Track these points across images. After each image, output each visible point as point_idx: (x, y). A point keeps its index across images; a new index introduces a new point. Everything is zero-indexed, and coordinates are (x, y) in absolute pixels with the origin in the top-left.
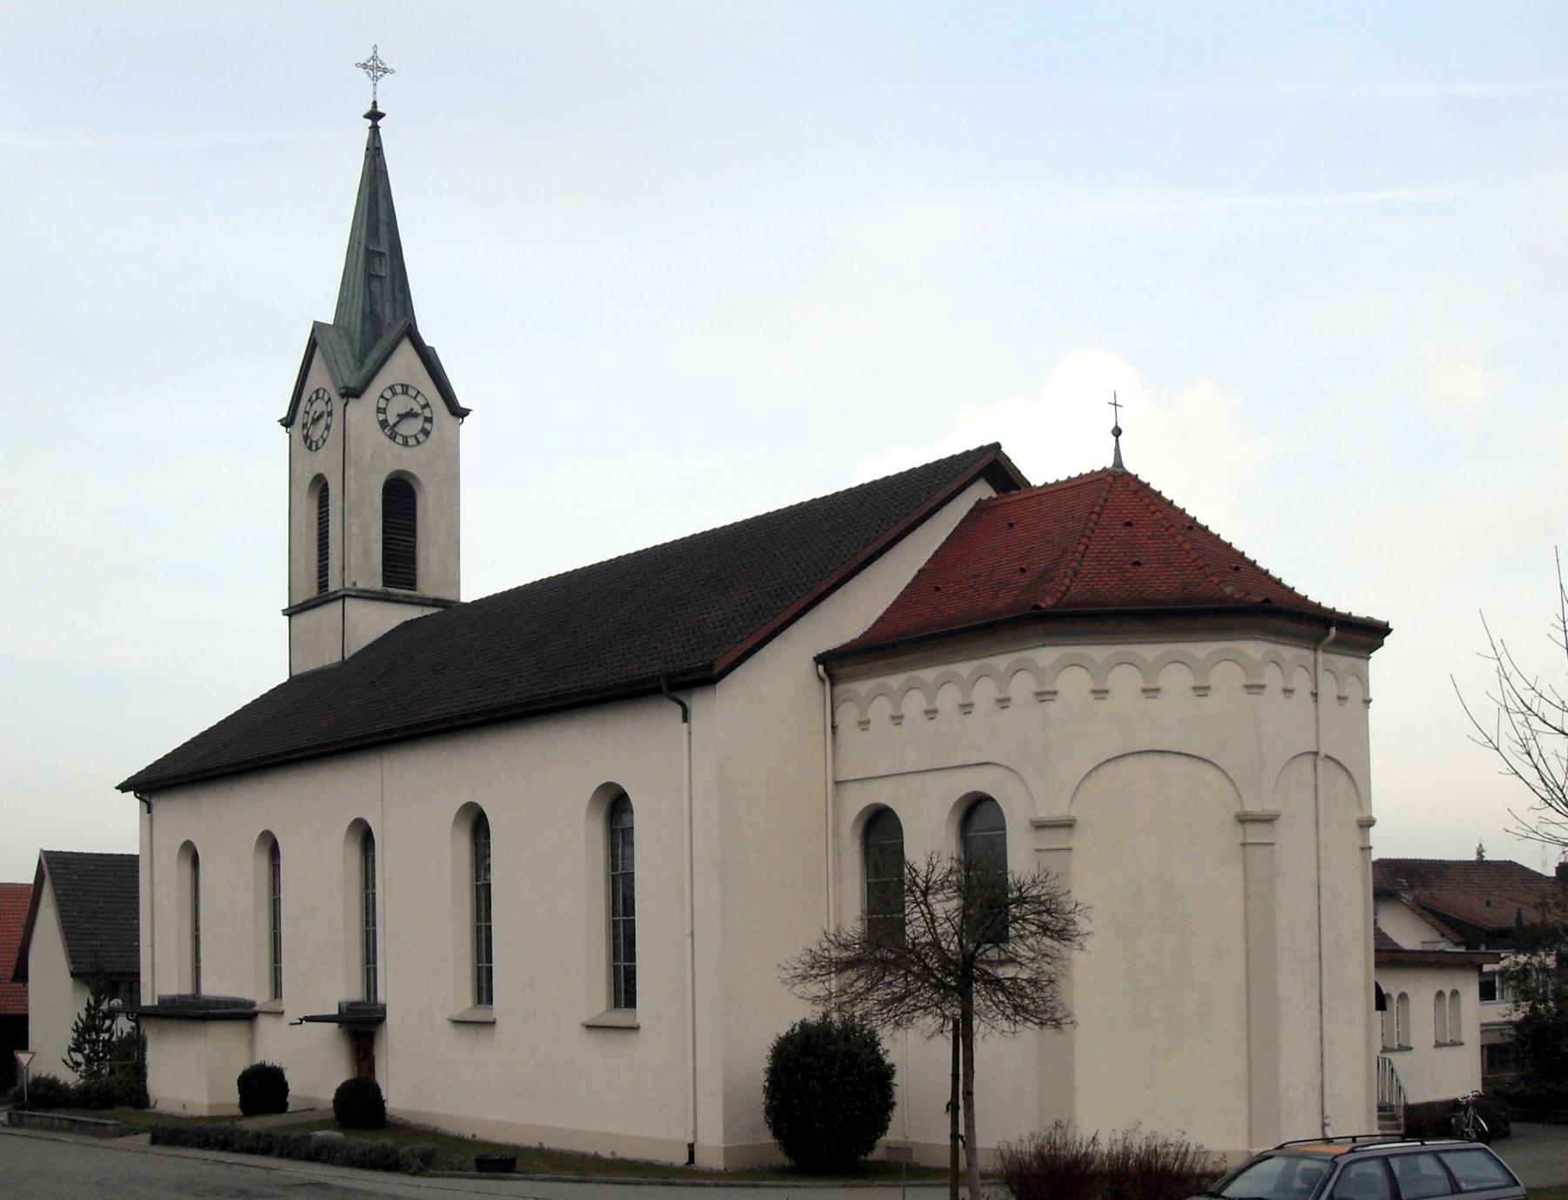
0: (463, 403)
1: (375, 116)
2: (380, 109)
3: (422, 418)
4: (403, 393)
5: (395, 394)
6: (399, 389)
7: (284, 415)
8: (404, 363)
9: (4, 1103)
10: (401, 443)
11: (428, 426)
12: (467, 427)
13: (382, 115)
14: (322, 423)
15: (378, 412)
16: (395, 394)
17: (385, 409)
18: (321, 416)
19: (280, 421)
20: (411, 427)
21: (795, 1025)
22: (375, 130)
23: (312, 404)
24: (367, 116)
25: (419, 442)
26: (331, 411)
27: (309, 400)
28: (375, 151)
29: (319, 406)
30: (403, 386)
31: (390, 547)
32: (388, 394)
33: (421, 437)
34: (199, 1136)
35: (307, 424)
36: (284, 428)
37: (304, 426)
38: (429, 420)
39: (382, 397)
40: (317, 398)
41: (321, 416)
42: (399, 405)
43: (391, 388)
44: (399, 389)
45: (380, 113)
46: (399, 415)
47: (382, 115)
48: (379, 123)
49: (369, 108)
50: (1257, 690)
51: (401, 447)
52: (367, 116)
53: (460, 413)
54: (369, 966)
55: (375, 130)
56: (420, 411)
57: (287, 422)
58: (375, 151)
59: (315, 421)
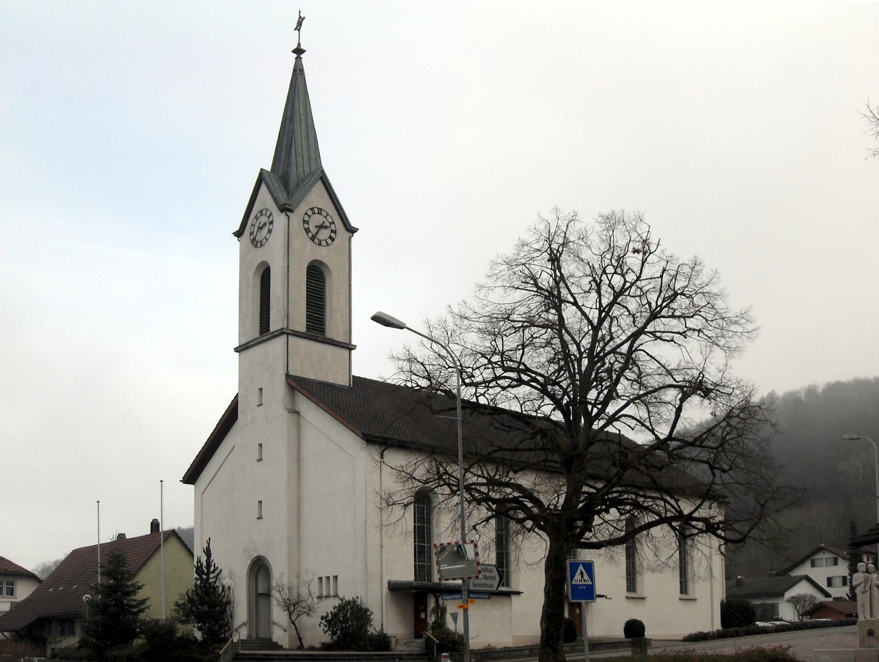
0: (354, 224)
1: (299, 51)
2: (303, 47)
3: (329, 230)
4: (318, 213)
5: (314, 213)
6: (316, 211)
7: (238, 228)
8: (316, 197)
9: (877, 621)
10: (317, 243)
11: (333, 235)
12: (356, 238)
13: (303, 51)
14: (266, 230)
15: (304, 223)
16: (314, 213)
17: (308, 222)
18: (265, 224)
19: (234, 233)
20: (324, 234)
21: (189, 590)
22: (298, 59)
23: (257, 220)
24: (294, 51)
25: (328, 245)
26: (273, 221)
27: (255, 217)
28: (298, 72)
29: (263, 219)
30: (318, 209)
31: (310, 304)
32: (310, 213)
33: (329, 241)
34: (380, 637)
35: (253, 232)
36: (237, 238)
37: (251, 233)
38: (334, 232)
39: (306, 213)
40: (261, 215)
41: (265, 224)
42: (317, 220)
43: (312, 209)
44: (316, 211)
45: (295, 53)
46: (316, 227)
47: (303, 51)
48: (302, 56)
49: (296, 46)
50: (503, 600)
51: (317, 246)
52: (294, 51)
53: (352, 231)
54: (507, 569)
55: (298, 59)
56: (329, 225)
57: (239, 234)
58: (298, 72)
59: (260, 228)
